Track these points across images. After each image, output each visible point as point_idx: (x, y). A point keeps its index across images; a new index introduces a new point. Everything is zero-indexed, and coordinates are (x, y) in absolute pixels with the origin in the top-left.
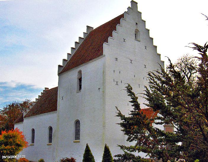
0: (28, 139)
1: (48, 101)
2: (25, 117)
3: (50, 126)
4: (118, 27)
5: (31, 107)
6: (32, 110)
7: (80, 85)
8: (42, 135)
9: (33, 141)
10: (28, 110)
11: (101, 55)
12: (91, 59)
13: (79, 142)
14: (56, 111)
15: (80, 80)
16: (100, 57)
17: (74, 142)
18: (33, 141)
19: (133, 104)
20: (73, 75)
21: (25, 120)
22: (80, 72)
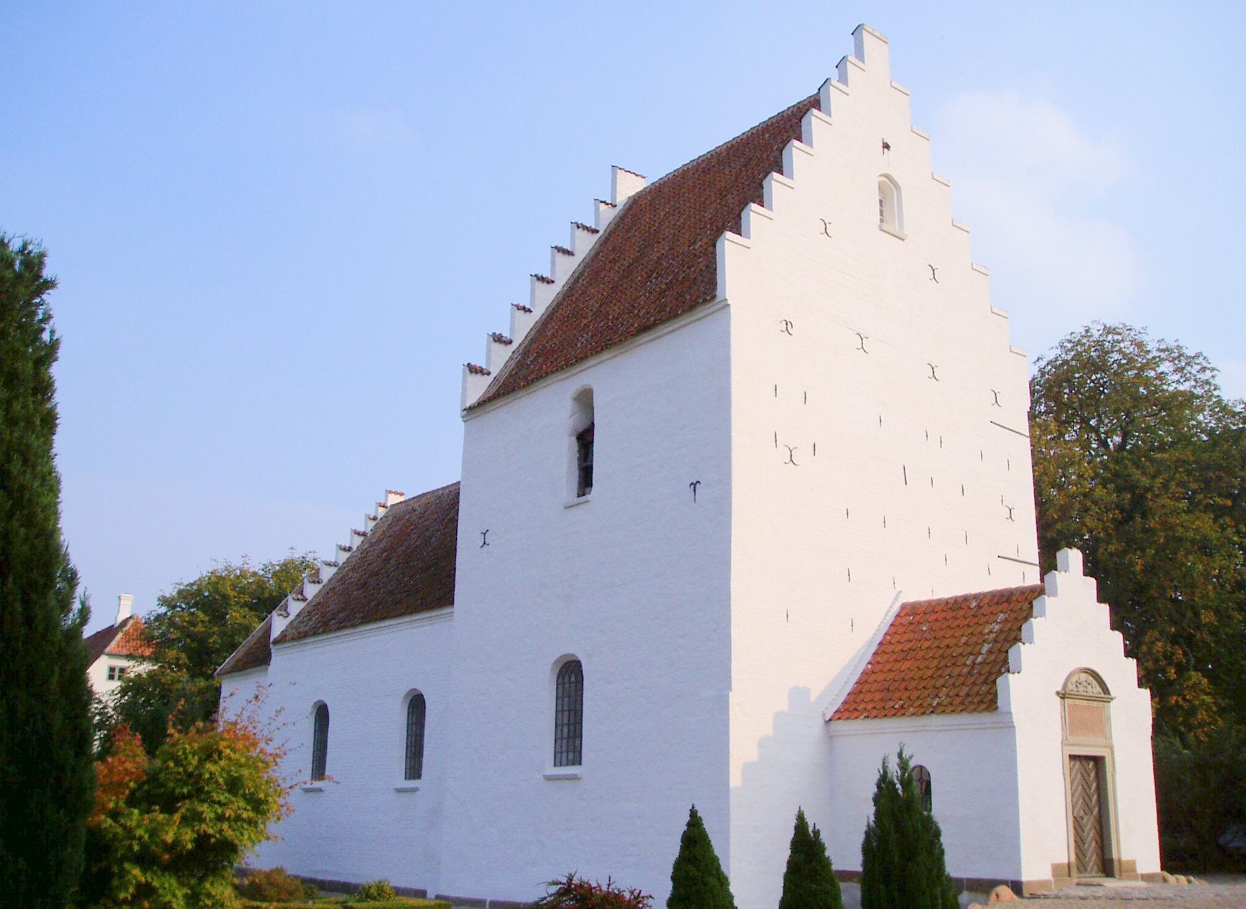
0: (294, 765)
1: (409, 565)
2: (282, 639)
3: (414, 690)
4: (796, 152)
5: (311, 591)
6: (331, 590)
7: (310, 896)
8: (368, 738)
9: (319, 769)
10: (295, 607)
11: (705, 301)
12: (645, 329)
13: (574, 778)
14: (448, 610)
15: (585, 439)
16: (700, 312)
17: (549, 778)
18: (319, 769)
19: (845, 852)
20: (549, 409)
21: (280, 659)
22: (585, 400)
